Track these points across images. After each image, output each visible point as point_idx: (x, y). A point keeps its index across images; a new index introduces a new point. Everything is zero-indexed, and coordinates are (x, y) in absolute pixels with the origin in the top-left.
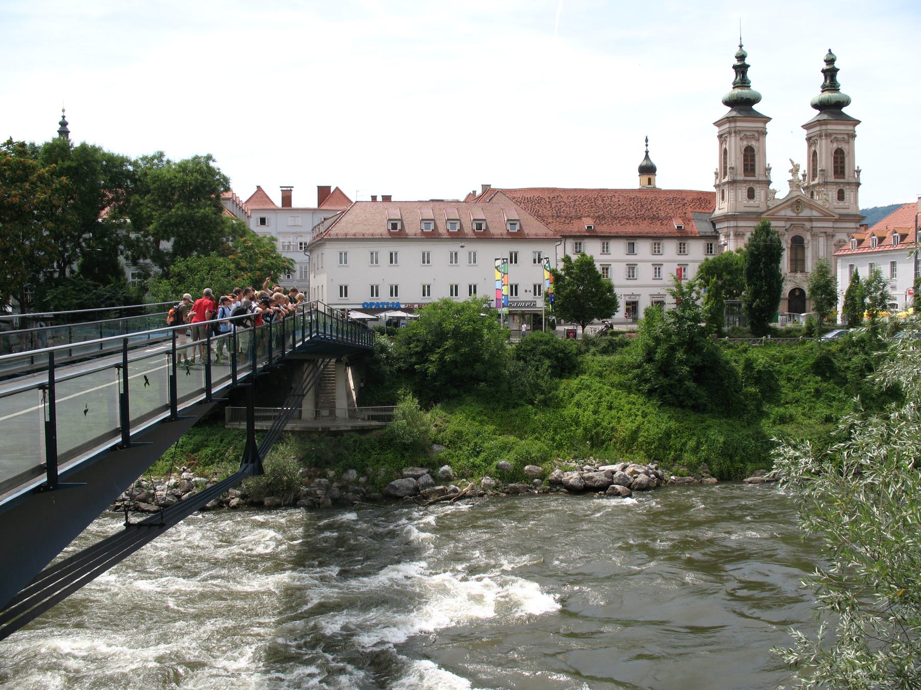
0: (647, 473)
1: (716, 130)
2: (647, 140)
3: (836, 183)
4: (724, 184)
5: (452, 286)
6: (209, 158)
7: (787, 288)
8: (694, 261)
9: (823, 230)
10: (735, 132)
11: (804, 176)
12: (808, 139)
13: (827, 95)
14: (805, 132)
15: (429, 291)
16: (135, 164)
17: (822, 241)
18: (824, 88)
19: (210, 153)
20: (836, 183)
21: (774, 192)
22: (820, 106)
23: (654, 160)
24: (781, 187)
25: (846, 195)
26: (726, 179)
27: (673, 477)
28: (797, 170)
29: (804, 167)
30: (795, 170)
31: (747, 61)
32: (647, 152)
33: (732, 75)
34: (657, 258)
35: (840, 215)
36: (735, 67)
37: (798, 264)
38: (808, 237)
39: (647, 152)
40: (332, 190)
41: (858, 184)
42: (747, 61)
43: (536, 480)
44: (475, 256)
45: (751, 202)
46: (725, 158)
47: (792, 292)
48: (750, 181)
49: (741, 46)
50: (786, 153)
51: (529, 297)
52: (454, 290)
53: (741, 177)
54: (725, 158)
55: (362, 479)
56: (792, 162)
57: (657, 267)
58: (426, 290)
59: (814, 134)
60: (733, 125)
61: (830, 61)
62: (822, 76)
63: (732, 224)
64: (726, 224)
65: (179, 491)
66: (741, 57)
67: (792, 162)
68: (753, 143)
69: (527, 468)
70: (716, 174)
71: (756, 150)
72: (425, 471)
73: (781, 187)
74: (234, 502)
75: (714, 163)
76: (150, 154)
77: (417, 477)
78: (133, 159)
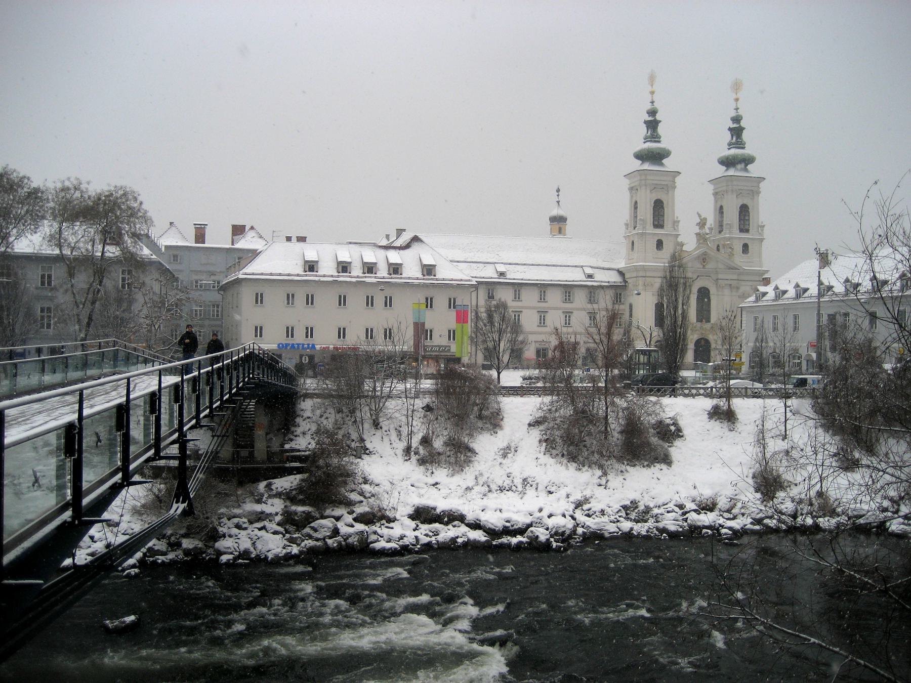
1: (711, 188)
2: (558, 191)
5: (340, 329)
7: (692, 338)
8: (578, 309)
9: (729, 282)
11: (711, 229)
12: (716, 194)
13: (733, 151)
14: (711, 187)
15: (288, 332)
17: (727, 291)
18: (731, 145)
22: (642, 156)
28: (705, 224)
29: (711, 221)
30: (702, 224)
31: (658, 117)
33: (643, 130)
34: (568, 306)
36: (730, 129)
37: (704, 313)
38: (713, 291)
41: (762, 240)
42: (658, 117)
44: (431, 301)
46: (636, 208)
47: (698, 343)
49: (652, 102)
50: (693, 204)
51: (444, 341)
52: (290, 332)
54: (636, 208)
56: (700, 216)
57: (568, 314)
58: (342, 333)
59: (720, 188)
62: (729, 134)
66: (653, 113)
67: (700, 216)
70: (627, 225)
71: (750, 208)
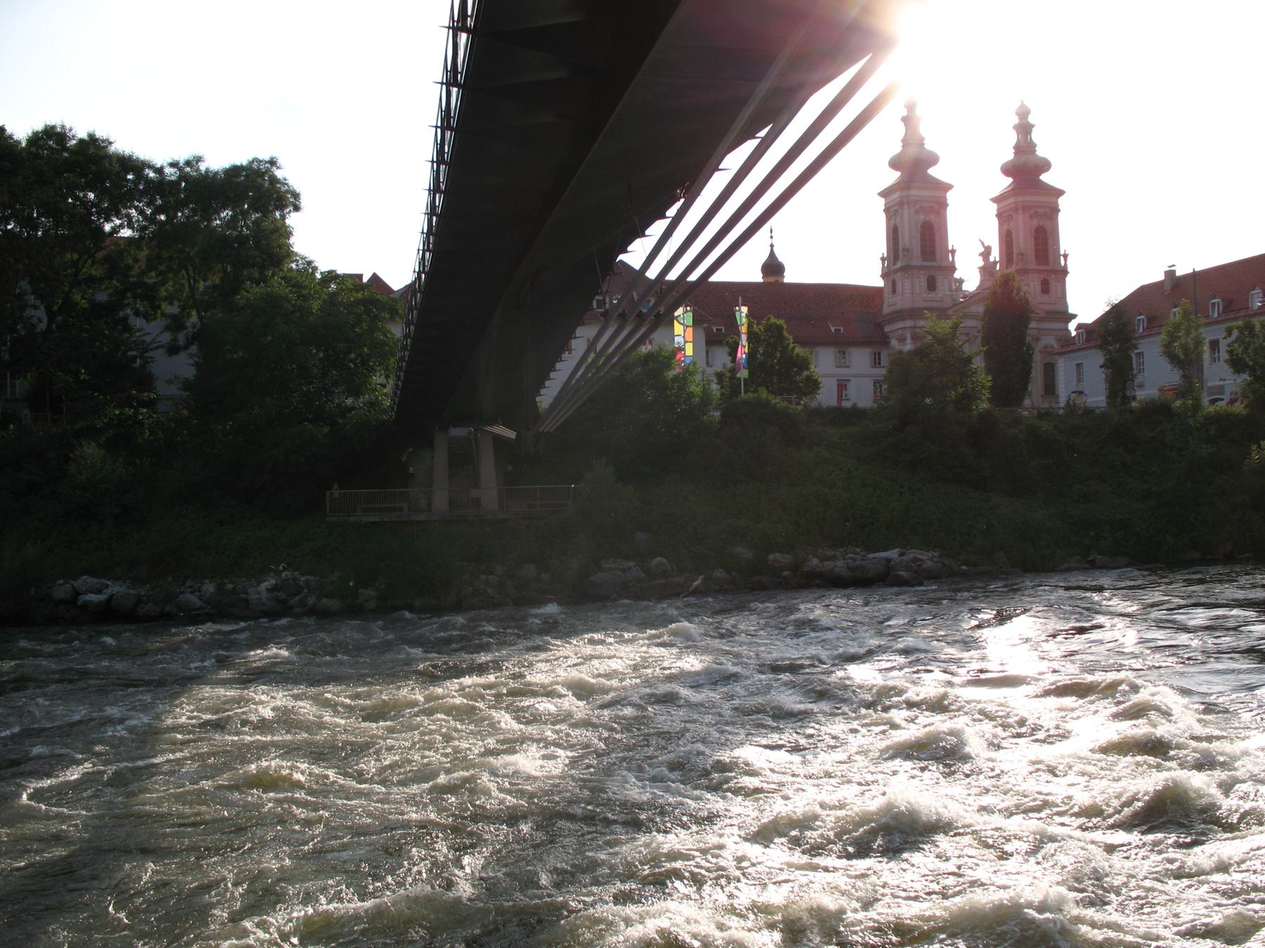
0: (931, 560)
3: (1039, 271)
4: (896, 271)
6: (273, 162)
10: (908, 203)
14: (995, 206)
16: (160, 171)
19: (274, 155)
20: (1039, 271)
21: (961, 281)
23: (781, 257)
24: (969, 275)
25: (1052, 288)
26: (899, 265)
27: (964, 567)
29: (995, 255)
30: (986, 253)
32: (772, 246)
35: (1048, 313)
39: (772, 246)
40: (365, 280)
43: (786, 573)
45: (932, 295)
48: (930, 267)
53: (917, 262)
55: (545, 576)
59: (1008, 209)
60: (905, 193)
61: (1023, 113)
63: (909, 323)
64: (900, 325)
65: (282, 595)
68: (932, 217)
69: (771, 557)
72: (632, 564)
73: (969, 275)
74: (372, 604)
75: (880, 246)
76: (182, 157)
77: (624, 571)
78: (158, 163)
